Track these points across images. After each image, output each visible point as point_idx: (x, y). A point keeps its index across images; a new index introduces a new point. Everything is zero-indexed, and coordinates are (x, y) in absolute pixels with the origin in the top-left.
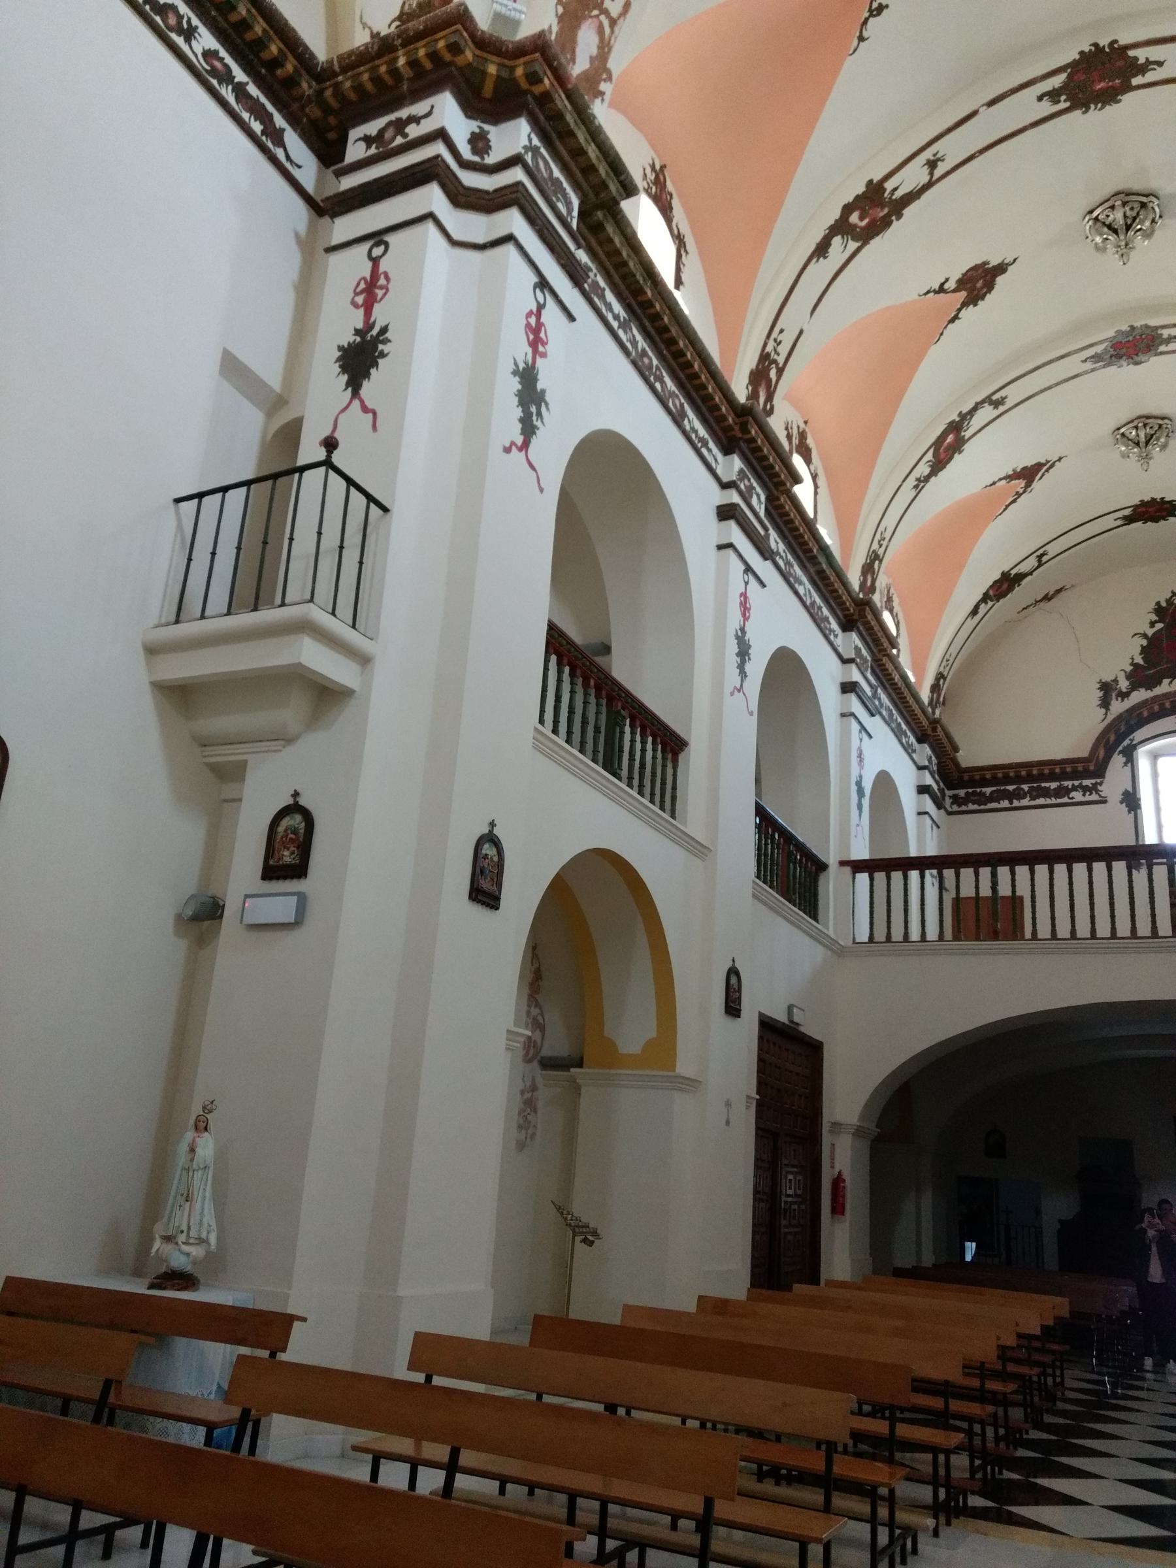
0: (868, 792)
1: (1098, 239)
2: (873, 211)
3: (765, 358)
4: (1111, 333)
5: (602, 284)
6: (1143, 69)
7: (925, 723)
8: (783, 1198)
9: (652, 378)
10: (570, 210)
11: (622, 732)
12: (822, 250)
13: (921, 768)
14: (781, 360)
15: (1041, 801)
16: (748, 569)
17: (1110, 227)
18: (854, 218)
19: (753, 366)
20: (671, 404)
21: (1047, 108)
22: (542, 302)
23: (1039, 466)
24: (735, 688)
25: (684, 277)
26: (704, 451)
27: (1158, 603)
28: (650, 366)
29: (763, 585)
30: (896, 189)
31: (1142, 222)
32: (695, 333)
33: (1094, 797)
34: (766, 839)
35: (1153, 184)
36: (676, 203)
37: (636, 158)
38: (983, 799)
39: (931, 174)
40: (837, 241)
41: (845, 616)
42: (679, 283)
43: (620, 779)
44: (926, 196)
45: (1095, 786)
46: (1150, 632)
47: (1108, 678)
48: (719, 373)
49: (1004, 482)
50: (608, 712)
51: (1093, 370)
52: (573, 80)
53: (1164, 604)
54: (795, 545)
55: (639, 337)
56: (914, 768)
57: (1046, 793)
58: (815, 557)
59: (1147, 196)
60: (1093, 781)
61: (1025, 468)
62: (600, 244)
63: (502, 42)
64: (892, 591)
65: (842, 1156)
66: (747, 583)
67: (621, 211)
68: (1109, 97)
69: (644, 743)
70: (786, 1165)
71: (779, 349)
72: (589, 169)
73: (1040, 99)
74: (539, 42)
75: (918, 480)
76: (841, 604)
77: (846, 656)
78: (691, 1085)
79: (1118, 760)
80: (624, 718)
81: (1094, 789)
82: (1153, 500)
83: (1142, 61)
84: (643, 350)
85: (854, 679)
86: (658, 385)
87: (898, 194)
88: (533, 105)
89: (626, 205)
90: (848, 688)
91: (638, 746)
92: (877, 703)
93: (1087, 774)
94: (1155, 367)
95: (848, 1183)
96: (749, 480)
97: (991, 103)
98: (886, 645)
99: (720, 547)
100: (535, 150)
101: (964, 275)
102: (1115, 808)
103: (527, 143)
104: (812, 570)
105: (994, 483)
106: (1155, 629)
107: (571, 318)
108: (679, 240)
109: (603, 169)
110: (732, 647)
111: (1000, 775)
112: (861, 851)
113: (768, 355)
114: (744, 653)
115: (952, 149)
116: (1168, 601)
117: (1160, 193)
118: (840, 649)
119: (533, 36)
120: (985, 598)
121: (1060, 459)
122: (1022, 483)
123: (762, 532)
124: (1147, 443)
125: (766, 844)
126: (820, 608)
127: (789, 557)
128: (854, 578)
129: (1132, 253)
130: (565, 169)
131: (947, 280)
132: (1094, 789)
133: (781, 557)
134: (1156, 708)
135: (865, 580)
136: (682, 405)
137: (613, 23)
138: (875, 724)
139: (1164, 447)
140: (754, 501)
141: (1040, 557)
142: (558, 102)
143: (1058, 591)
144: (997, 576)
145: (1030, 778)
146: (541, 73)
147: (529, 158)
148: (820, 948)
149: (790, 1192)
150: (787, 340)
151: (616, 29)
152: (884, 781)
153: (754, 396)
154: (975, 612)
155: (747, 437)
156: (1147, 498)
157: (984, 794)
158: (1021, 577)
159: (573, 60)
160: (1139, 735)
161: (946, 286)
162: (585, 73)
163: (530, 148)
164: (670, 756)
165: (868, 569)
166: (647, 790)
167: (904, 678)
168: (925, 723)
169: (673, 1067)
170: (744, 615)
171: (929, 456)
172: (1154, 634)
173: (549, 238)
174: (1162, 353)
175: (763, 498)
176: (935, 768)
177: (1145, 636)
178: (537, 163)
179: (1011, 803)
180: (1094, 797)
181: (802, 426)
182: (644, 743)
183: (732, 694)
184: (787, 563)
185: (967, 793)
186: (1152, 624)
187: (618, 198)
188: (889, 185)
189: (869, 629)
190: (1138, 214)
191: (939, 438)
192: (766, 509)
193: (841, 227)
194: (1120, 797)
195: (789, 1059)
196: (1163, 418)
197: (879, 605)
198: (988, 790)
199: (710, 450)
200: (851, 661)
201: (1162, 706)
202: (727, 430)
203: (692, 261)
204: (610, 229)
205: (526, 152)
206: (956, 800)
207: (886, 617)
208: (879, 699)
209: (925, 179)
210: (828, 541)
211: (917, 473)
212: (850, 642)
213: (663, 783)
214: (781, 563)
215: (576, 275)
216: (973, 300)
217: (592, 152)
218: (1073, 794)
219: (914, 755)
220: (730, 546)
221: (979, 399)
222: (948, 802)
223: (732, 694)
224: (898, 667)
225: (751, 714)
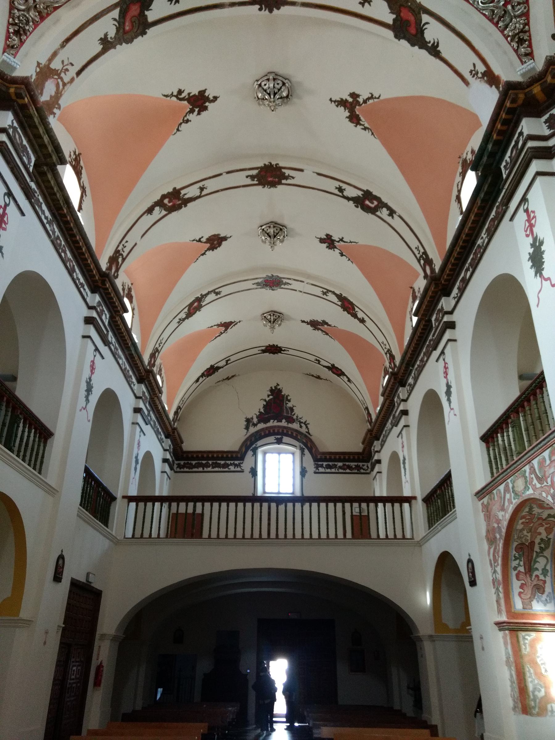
0: (140, 461)
1: (263, 238)
2: (174, 201)
3: (117, 252)
4: (265, 276)
5: (41, 200)
6: (287, 178)
7: (170, 429)
8: (69, 681)
9: (60, 251)
10: (30, 161)
11: (18, 426)
12: (150, 211)
13: (165, 450)
14: (125, 254)
15: (216, 469)
16: (97, 349)
17: (268, 234)
18: (166, 201)
19: (111, 255)
20: (68, 265)
21: (249, 181)
22: (8, 202)
23: (231, 323)
24: (83, 407)
25: (83, 206)
26: (82, 289)
27: (271, 388)
28: (61, 244)
29: (103, 358)
30: (186, 194)
31: (280, 236)
32: (86, 235)
33: (239, 469)
34: (88, 484)
35: (285, 222)
36: (84, 171)
37: (68, 146)
38: (191, 466)
39: (201, 193)
40: (157, 209)
41: (140, 376)
42: (80, 208)
43: (13, 452)
44: (197, 201)
45: (240, 464)
46: (267, 399)
47: (249, 417)
48: (95, 255)
49: (216, 327)
50: (11, 416)
51: (256, 288)
52: (41, 104)
53: (274, 388)
54: (120, 341)
55: (56, 230)
56: (162, 450)
57: (219, 466)
58: (129, 347)
59: (283, 226)
60: (239, 462)
61: (225, 323)
62: (43, 182)
63: (4, 74)
64: (162, 366)
65: (104, 653)
66: (95, 356)
67: (57, 169)
68: (273, 185)
69: (29, 432)
70: (73, 662)
71: (125, 249)
72: (43, 146)
73: (247, 177)
74: (25, 81)
75: (180, 319)
76: (139, 370)
77: (138, 395)
78: (28, 623)
79: (250, 453)
80: (21, 419)
81: (239, 465)
82: (274, 345)
83: (287, 174)
84: (58, 236)
85: (140, 407)
86: (63, 254)
87: (186, 197)
88: (17, 108)
89: (59, 167)
90: (137, 410)
91: (26, 434)
92: (149, 418)
93: (237, 459)
94: (279, 293)
95: (105, 669)
96: (102, 307)
97: (228, 173)
98: (157, 392)
99: (84, 337)
100: (15, 129)
101: (210, 237)
102: (247, 474)
103: (11, 124)
104: (127, 353)
105: (212, 327)
106: (269, 398)
107: (23, 214)
108: (83, 189)
109: (50, 148)
110: (84, 386)
111: (200, 456)
112: (133, 492)
113: (119, 251)
114: (89, 390)
115: (211, 185)
116: (275, 387)
117: (288, 227)
118: (135, 391)
119: (23, 77)
120: (203, 375)
121: (240, 322)
122: (223, 329)
123: (105, 332)
124: (274, 322)
125: (87, 487)
126: (128, 371)
127: (117, 345)
128: (146, 358)
129: (275, 247)
130: (29, 141)
131: (202, 237)
132: (239, 465)
133: (113, 345)
134: (267, 432)
135: (151, 361)
136: (74, 266)
137: (64, 84)
138: (148, 429)
139: (280, 325)
140: (104, 317)
141: (227, 361)
142: (31, 111)
143: (233, 376)
144: (209, 367)
145: (213, 458)
146: (24, 95)
147: (11, 131)
148: (108, 541)
149: (73, 677)
150: (129, 246)
151: (66, 88)
152: (148, 456)
153: (110, 268)
154: (197, 380)
155: (104, 287)
156: (271, 344)
157: (192, 464)
158: (218, 368)
159: (41, 94)
160: (259, 443)
161: (202, 240)
162: (47, 101)
163: (11, 127)
164: (43, 440)
165: (153, 356)
166: (27, 458)
167: (163, 408)
168: (170, 429)
169: (17, 613)
170: (91, 371)
171: (186, 310)
173: (17, 173)
174: (282, 288)
175: (108, 316)
176: (172, 450)
177: (265, 400)
178: (15, 134)
179: (203, 469)
180: (239, 469)
181: (130, 285)
182: (29, 432)
183: (81, 410)
184: (116, 348)
185: (184, 463)
186: (268, 396)
187: (56, 163)
188: (183, 192)
189: (150, 384)
190: (281, 88)
191: (191, 303)
192: (109, 322)
193: (159, 203)
194: (249, 470)
195: (84, 599)
196: (280, 314)
197: (155, 372)
198: (194, 462)
199: (85, 290)
200: (140, 398)
201: (269, 431)
202: (95, 281)
203: (88, 200)
204: (50, 176)
205: (10, 128)
206: (179, 466)
207: (158, 378)
208: (151, 417)
209: (198, 194)
210: (136, 341)
211: (180, 316)
212: (141, 389)
213: (37, 455)
214: (113, 348)
215: (28, 194)
216: (212, 248)
217: (46, 139)
218: (230, 467)
219: (163, 444)
220: (89, 337)
221: (210, 290)
222: (175, 466)
223: (81, 410)
224: (161, 402)
225: (89, 421)
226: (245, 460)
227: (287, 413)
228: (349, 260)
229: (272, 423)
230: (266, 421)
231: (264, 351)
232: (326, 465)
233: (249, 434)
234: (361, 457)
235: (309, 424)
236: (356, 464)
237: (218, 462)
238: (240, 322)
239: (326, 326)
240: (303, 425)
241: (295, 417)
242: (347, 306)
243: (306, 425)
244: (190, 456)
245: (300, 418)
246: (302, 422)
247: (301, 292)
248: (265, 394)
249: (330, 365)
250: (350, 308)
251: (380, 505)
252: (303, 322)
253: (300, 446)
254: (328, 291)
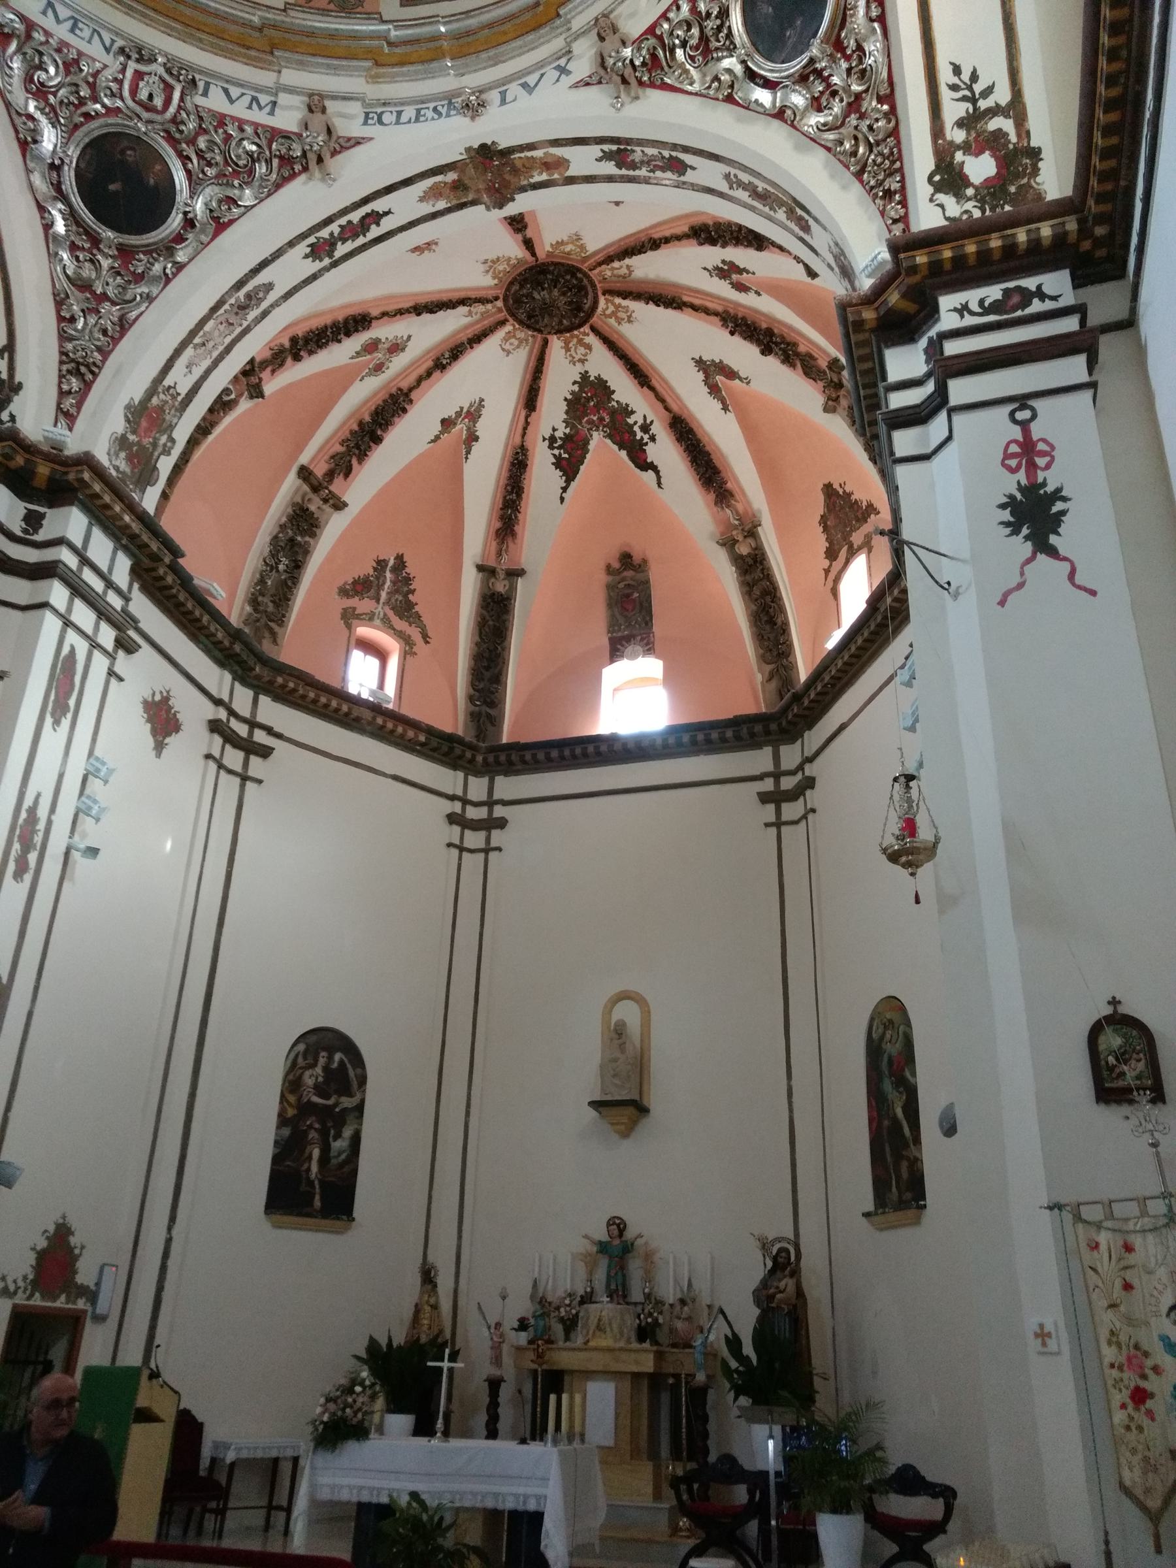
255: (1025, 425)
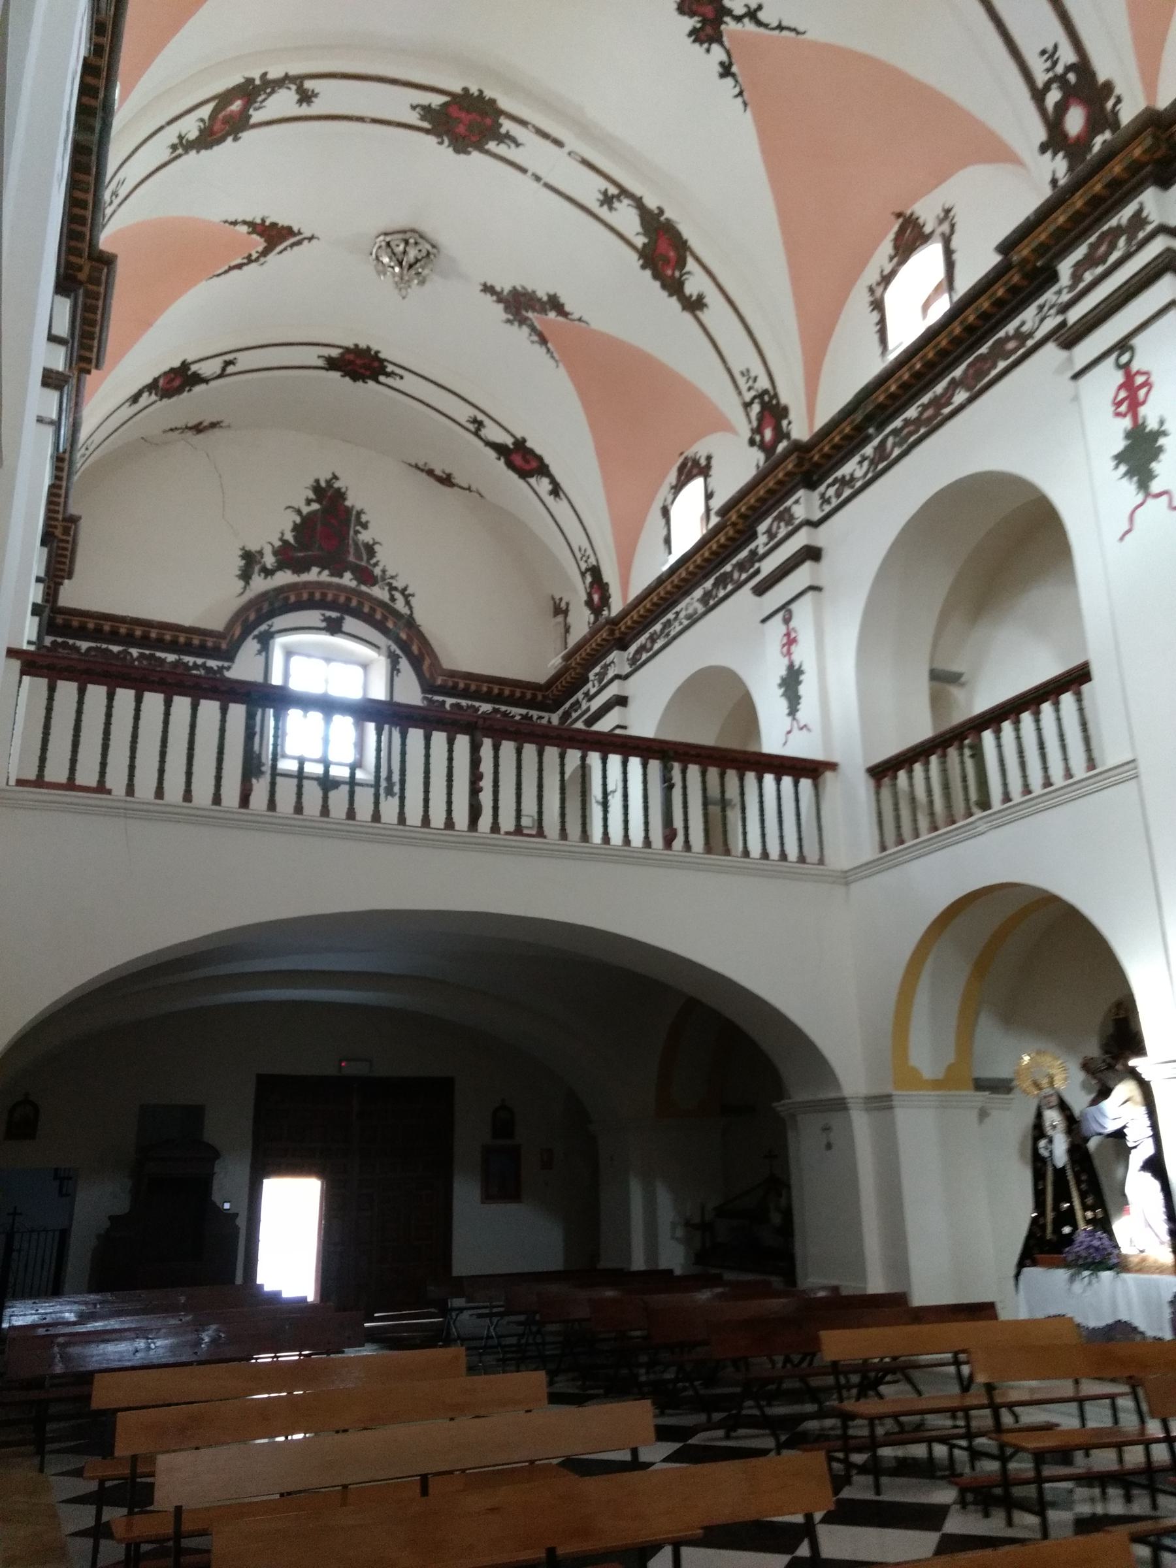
27: (317, 481)
46: (305, 510)
47: (253, 547)
53: (323, 484)
60: (220, 663)
61: (274, 225)
79: (251, 646)
82: (369, 349)
105: (235, 223)
116: (328, 482)
120: (152, 387)
122: (259, 243)
124: (411, 266)
134: (305, 596)
143: (213, 425)
144: (176, 364)
154: (135, 399)
157: (77, 649)
158: (197, 379)
160: (279, 622)
171: (205, 112)
172: (309, 514)
177: (299, 512)
185: (54, 643)
226: (237, 660)
227: (360, 558)
228: (741, 94)
229: (313, 575)
230: (300, 567)
231: (332, 364)
232: (452, 705)
233: (250, 594)
234: (540, 697)
235: (413, 595)
236: (524, 711)
237: (158, 654)
238: (311, 239)
239: (552, 315)
240: (397, 595)
241: (377, 571)
242: (664, 251)
243: (407, 598)
244: (75, 624)
245: (392, 577)
246: (396, 589)
247: (538, 178)
248: (300, 496)
249: (509, 441)
250: (667, 261)
251: (769, 779)
252: (488, 289)
253: (389, 647)
254: (624, 192)
255: (1126, 367)
